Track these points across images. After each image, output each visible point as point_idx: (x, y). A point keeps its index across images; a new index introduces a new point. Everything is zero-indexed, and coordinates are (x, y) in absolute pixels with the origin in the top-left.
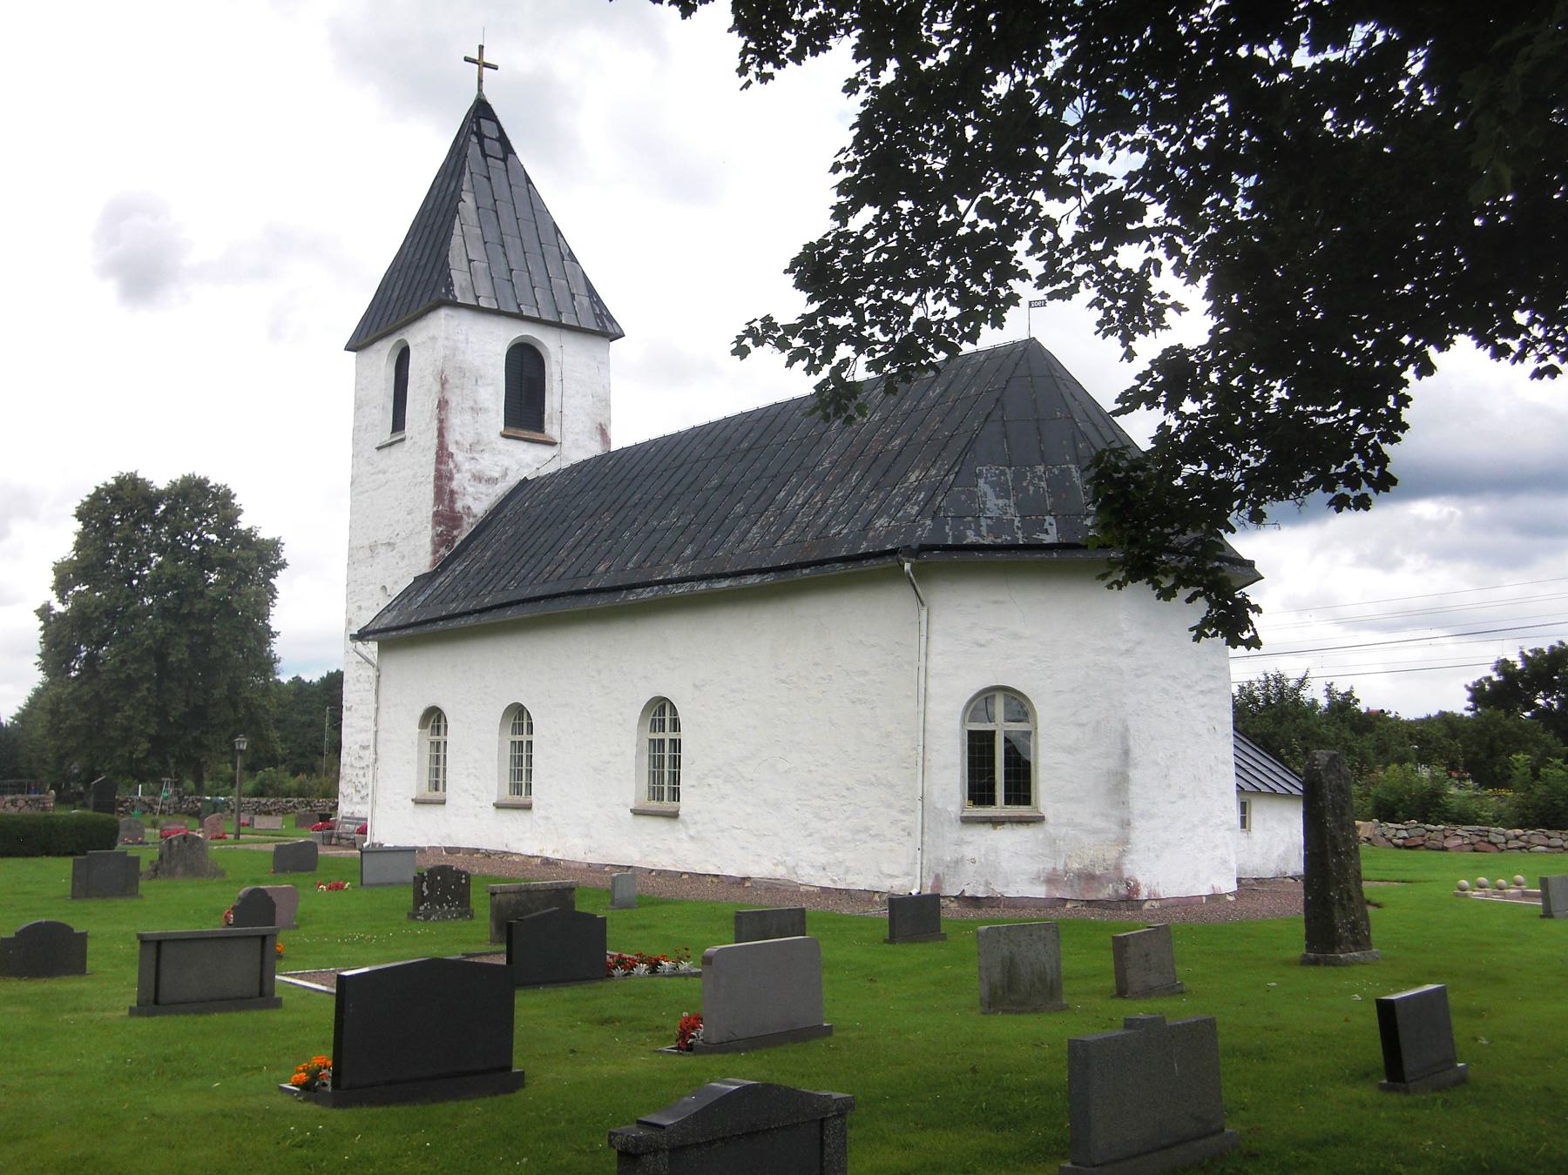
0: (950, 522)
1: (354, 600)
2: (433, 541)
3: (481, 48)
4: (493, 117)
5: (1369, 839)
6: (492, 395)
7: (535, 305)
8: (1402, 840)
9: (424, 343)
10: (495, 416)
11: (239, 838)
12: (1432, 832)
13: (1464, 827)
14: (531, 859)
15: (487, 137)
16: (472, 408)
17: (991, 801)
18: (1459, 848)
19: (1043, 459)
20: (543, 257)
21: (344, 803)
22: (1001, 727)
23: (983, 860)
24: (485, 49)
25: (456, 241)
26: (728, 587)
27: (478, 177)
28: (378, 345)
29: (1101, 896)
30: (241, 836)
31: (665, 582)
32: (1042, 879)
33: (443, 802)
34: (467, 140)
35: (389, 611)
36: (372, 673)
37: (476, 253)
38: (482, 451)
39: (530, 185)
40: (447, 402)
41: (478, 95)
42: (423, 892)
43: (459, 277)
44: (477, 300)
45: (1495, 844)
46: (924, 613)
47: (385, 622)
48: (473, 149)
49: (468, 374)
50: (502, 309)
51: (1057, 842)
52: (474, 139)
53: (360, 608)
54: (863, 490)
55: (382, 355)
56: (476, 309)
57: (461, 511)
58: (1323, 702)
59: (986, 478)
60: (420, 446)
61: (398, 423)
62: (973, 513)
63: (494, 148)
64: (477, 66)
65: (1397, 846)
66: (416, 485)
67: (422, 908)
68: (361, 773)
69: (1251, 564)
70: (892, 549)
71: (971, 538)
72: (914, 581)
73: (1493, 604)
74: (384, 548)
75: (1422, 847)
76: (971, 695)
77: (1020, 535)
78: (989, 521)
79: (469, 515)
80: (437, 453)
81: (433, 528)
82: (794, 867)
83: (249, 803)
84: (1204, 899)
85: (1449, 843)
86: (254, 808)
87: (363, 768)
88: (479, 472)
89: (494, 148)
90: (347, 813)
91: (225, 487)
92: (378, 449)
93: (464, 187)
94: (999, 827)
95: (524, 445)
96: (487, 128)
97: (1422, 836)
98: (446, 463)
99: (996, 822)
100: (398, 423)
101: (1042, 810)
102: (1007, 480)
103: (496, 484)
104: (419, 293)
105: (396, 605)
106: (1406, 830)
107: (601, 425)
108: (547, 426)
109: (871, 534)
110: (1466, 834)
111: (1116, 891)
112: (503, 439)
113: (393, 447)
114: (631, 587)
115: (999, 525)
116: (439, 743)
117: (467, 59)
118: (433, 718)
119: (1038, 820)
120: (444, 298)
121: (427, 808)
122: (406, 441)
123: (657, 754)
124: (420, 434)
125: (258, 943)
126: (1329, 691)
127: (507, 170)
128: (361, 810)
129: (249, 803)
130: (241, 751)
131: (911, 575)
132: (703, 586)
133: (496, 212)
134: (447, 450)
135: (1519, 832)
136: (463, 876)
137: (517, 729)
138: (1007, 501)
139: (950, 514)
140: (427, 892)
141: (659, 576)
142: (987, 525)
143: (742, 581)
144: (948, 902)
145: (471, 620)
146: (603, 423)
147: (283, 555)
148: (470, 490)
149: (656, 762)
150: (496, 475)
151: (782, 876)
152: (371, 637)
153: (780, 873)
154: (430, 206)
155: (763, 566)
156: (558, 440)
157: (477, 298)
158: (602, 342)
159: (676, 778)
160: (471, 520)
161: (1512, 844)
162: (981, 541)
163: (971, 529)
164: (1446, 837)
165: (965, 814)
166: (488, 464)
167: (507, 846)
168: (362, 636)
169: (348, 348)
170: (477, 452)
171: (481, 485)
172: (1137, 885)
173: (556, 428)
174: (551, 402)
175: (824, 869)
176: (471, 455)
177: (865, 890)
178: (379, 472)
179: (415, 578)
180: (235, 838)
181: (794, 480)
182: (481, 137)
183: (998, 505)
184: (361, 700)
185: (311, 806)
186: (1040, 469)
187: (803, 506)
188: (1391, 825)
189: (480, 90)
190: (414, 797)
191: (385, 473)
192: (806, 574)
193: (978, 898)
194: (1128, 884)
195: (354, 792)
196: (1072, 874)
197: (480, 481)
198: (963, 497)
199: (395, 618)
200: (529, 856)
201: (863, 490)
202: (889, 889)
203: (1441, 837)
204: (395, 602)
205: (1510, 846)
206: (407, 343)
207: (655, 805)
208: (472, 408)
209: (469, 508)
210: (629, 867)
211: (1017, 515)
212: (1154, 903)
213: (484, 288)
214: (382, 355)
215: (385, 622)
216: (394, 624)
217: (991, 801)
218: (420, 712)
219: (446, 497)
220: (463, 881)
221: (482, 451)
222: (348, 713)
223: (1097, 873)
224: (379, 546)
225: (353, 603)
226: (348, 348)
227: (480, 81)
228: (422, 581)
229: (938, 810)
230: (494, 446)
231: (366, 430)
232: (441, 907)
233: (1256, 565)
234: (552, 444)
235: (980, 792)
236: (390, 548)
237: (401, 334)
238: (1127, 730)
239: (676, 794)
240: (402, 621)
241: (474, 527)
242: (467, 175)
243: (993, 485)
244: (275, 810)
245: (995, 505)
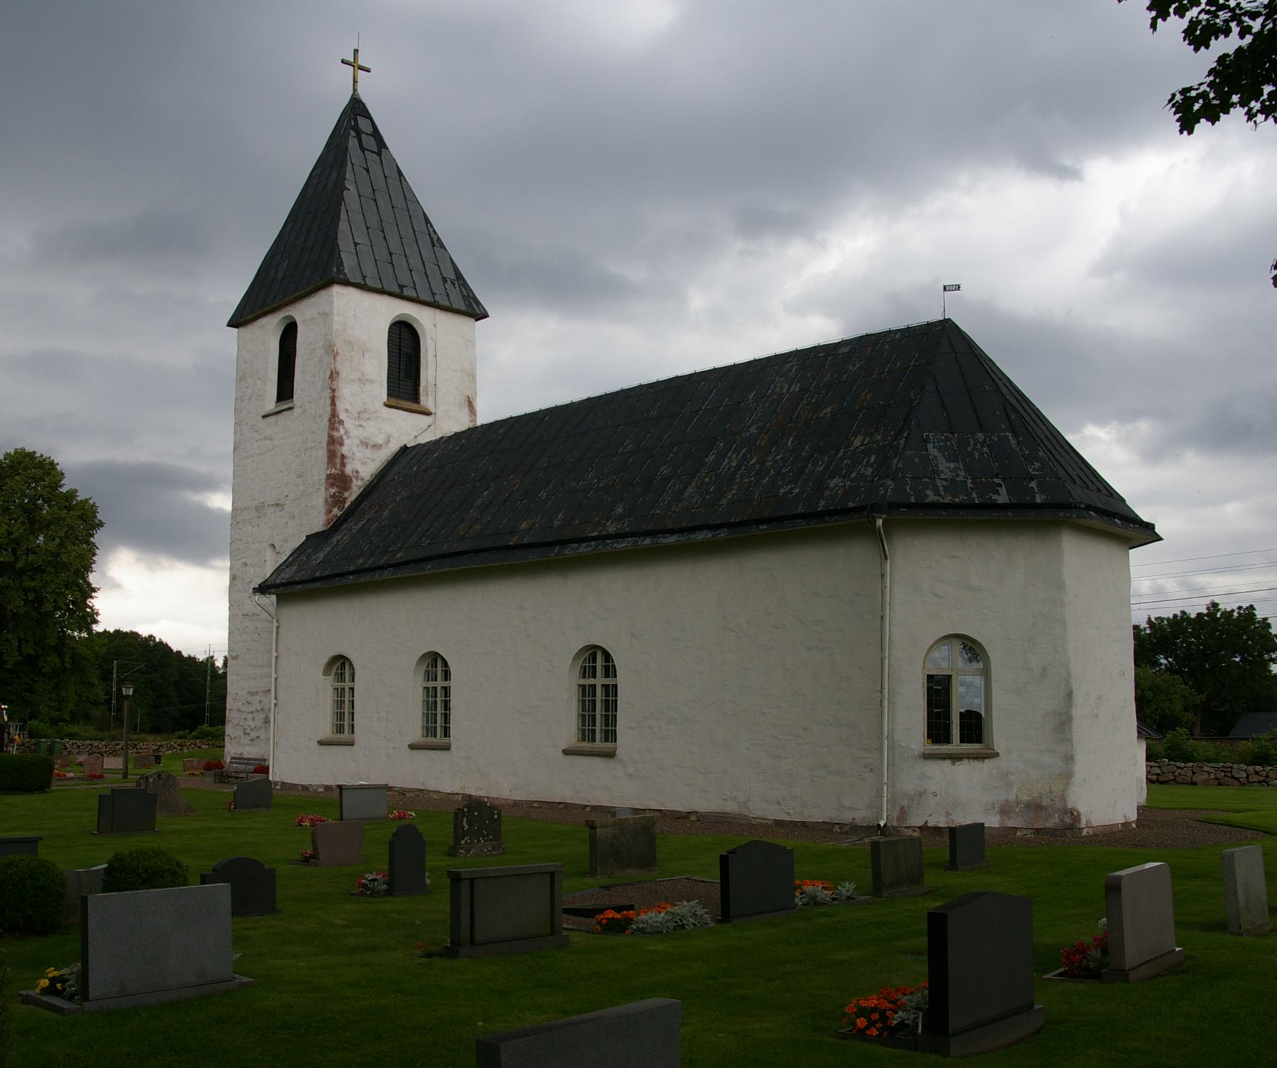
0: (909, 482)
1: (238, 557)
2: (326, 501)
3: (356, 51)
4: (367, 115)
7: (413, 286)
8: (1155, 776)
9: (313, 319)
10: (380, 390)
11: (127, 778)
12: (1182, 769)
13: (1210, 765)
14: (450, 796)
15: (364, 133)
16: (360, 380)
17: (947, 739)
19: (981, 429)
20: (417, 242)
21: (231, 744)
23: (943, 794)
24: (359, 53)
25: (343, 226)
26: (677, 541)
27: (358, 168)
28: (263, 321)
29: (1048, 825)
30: (129, 777)
31: (603, 538)
32: (996, 810)
34: (347, 135)
35: (287, 567)
37: (362, 239)
38: (368, 419)
39: (402, 178)
40: (338, 373)
41: (353, 95)
42: (464, 827)
43: (348, 260)
44: (364, 280)
45: (1237, 779)
47: (285, 577)
49: (355, 348)
51: (1009, 776)
52: (353, 133)
53: (246, 564)
54: (804, 454)
55: (268, 331)
56: (363, 287)
57: (351, 475)
59: (934, 443)
60: (310, 414)
61: (285, 390)
62: (929, 475)
63: (370, 142)
64: (352, 68)
66: (306, 450)
67: (463, 842)
68: (250, 716)
70: (855, 507)
71: (931, 497)
72: (883, 536)
74: (272, 509)
75: (1172, 782)
77: (974, 495)
78: (945, 483)
79: (357, 478)
80: (330, 420)
81: (327, 489)
82: (745, 802)
83: (83, 745)
86: (88, 749)
87: (252, 712)
88: (366, 438)
89: (370, 142)
90: (235, 754)
91: (49, 458)
92: (264, 417)
93: (347, 177)
94: (957, 763)
96: (363, 124)
97: (1174, 772)
98: (338, 430)
99: (955, 758)
100: (285, 390)
102: (953, 445)
103: (380, 450)
105: (294, 560)
106: (1159, 767)
107: (468, 398)
108: (422, 398)
109: (827, 493)
110: (1212, 770)
111: (1062, 820)
112: (387, 408)
113: (280, 415)
114: (565, 543)
115: (953, 486)
116: (343, 689)
117: (343, 62)
118: (340, 665)
120: (335, 276)
122: (295, 409)
123: (587, 698)
124: (310, 402)
127: (382, 163)
128: (251, 751)
129: (83, 745)
130: (127, 696)
131: (882, 530)
132: (648, 541)
133: (375, 200)
134: (338, 417)
135: (1258, 768)
136: (496, 812)
137: (340, 677)
138: (957, 464)
139: (907, 475)
140: (467, 827)
141: (593, 532)
142: (943, 486)
143: (692, 536)
144: (911, 832)
145: (386, 575)
146: (470, 396)
147: (99, 516)
148: (358, 455)
150: (380, 442)
151: (732, 810)
152: (273, 590)
153: (732, 807)
155: (711, 522)
156: (434, 412)
157: (364, 277)
158: (467, 322)
160: (360, 483)
161: (1256, 778)
162: (941, 500)
163: (929, 489)
166: (373, 431)
167: (423, 784)
169: (231, 324)
170: (364, 420)
171: (367, 451)
172: (1079, 815)
173: (431, 399)
175: (779, 803)
176: (358, 423)
177: (824, 822)
178: (265, 438)
179: (307, 536)
180: (123, 778)
181: (721, 444)
182: (359, 133)
183: (949, 468)
184: (248, 649)
185: (137, 749)
186: (980, 436)
187: (738, 467)
189: (355, 90)
191: (271, 439)
192: (763, 530)
193: (939, 828)
194: (1072, 814)
195: (242, 735)
196: (1023, 806)
197: (367, 446)
198: (917, 460)
199: (296, 572)
200: (449, 794)
201: (804, 454)
202: (851, 821)
203: (1190, 774)
204: (291, 559)
205: (1251, 780)
206: (293, 318)
207: (587, 745)
208: (360, 380)
209: (357, 472)
211: (969, 478)
213: (369, 269)
214: (268, 331)
215: (285, 576)
216: (297, 579)
217: (947, 739)
218: (324, 660)
219: (338, 461)
220: (496, 816)
221: (368, 419)
222: (234, 662)
223: (1045, 803)
224: (267, 507)
225: (237, 560)
226: (231, 324)
227: (355, 82)
228: (314, 541)
229: (902, 747)
230: (378, 414)
231: (250, 399)
232: (479, 841)
233: (1156, 527)
234: (427, 413)
235: (937, 729)
236: (278, 509)
237: (288, 311)
238: (1070, 674)
240: (305, 575)
241: (362, 489)
242: (349, 166)
243: (940, 449)
244: (106, 752)
245: (947, 468)
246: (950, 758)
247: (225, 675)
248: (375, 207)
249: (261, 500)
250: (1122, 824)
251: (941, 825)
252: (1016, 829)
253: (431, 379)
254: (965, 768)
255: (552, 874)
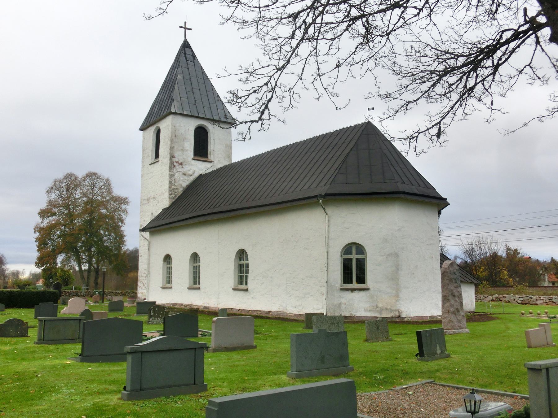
3: (185, 23)
5: (509, 301)
6: (190, 145)
10: (191, 154)
17: (351, 282)
18: (542, 304)
20: (207, 96)
22: (354, 257)
25: (176, 90)
28: (150, 128)
33: (171, 288)
36: (146, 243)
45: (555, 303)
46: (327, 217)
48: (183, 59)
50: (192, 115)
52: (183, 55)
58: (504, 255)
61: (157, 156)
65: (519, 304)
67: (151, 319)
69: (445, 199)
73: (548, 217)
76: (344, 246)
84: (428, 317)
85: (538, 302)
92: (150, 164)
95: (201, 162)
99: (353, 290)
101: (368, 286)
104: (163, 109)
108: (209, 156)
119: (367, 289)
121: (166, 290)
125: (79, 321)
126: (508, 249)
149: (241, 272)
154: (168, 79)
156: (213, 160)
159: (247, 277)
164: (537, 300)
165: (341, 287)
168: (144, 230)
174: (211, 147)
178: (151, 173)
188: (517, 296)
190: (161, 286)
194: (399, 312)
206: (159, 127)
210: (232, 309)
212: (409, 318)
214: (151, 131)
217: (351, 282)
228: (165, 210)
232: (158, 319)
234: (211, 162)
235: (347, 278)
236: (155, 199)
239: (247, 283)
246: (351, 290)
247: (537, 286)
248: (190, 83)
249: (149, 196)
250: (429, 316)
251: (347, 316)
252: (378, 317)
253: (212, 148)
254: (356, 294)
255: (80, 320)
